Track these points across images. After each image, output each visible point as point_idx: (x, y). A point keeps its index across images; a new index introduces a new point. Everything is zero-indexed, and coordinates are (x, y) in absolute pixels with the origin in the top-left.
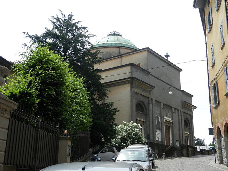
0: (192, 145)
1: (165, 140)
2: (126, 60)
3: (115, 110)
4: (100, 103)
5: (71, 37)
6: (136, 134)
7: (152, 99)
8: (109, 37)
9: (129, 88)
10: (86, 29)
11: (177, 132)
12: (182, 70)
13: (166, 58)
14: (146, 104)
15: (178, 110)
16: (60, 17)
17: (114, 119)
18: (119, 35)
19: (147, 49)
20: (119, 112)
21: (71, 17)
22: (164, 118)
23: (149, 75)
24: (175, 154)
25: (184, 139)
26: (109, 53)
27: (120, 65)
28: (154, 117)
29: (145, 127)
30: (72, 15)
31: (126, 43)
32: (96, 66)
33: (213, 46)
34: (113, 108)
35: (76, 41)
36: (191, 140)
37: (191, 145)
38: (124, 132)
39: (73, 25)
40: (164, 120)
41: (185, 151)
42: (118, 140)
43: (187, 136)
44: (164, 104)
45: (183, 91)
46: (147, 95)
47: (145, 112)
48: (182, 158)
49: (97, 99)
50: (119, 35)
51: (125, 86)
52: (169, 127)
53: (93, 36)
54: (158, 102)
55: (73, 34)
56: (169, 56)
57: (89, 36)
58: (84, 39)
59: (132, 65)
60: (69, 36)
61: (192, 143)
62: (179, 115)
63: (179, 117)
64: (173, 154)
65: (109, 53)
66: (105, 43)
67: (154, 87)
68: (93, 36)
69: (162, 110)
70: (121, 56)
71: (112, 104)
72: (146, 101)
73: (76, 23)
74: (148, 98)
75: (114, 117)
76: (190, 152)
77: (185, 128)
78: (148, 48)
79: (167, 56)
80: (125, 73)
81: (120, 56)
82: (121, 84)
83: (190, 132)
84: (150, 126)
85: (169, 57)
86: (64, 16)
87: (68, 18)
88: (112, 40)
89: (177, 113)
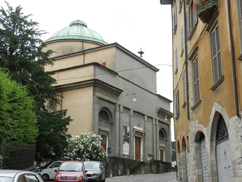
0: (168, 160)
1: (134, 154)
2: (90, 58)
3: (69, 120)
4: (52, 111)
5: (18, 34)
6: (94, 148)
7: (119, 106)
8: (71, 27)
9: (92, 91)
10: (37, 24)
11: (151, 145)
12: (159, 70)
13: (139, 55)
14: (112, 111)
15: (152, 118)
16: (6, 9)
17: (66, 130)
18: (84, 25)
19: (116, 45)
20: (73, 121)
21: (20, 10)
22: (134, 129)
23: (117, 76)
24: (142, 171)
25: (159, 153)
26: (70, 48)
27: (83, 64)
28: (122, 128)
29: (110, 139)
30: (20, 7)
31: (91, 36)
32: (48, 68)
33: (177, 51)
34: (66, 117)
35: (25, 38)
36: (167, 155)
37: (167, 160)
38: (80, 144)
39: (22, 20)
40: (134, 130)
41: (154, 168)
42: (73, 153)
43: (163, 149)
44: (134, 111)
45: (159, 96)
46: (114, 101)
47: (110, 120)
48: (150, 175)
49: (47, 107)
50: (84, 25)
51: (87, 89)
52: (140, 138)
53: (44, 33)
54: (127, 109)
55: (21, 30)
56: (143, 53)
57: (40, 32)
58: (35, 37)
59: (95, 64)
60: (17, 33)
61: (168, 158)
62: (153, 124)
63: (153, 127)
64: (141, 170)
65: (70, 48)
66: (66, 35)
67: (123, 91)
68: (44, 33)
69: (132, 118)
70: (84, 52)
71: (65, 112)
72: (111, 107)
73: (25, 17)
74: (115, 104)
75: (67, 127)
76: (161, 168)
77: (160, 140)
78: (116, 43)
79: (141, 53)
80: (87, 74)
81: (83, 52)
82: (82, 87)
83: (166, 145)
84: (115, 137)
85: (143, 55)
86: (11, 9)
87: (17, 11)
88: (75, 32)
89: (150, 123)
